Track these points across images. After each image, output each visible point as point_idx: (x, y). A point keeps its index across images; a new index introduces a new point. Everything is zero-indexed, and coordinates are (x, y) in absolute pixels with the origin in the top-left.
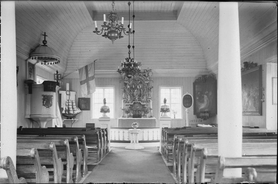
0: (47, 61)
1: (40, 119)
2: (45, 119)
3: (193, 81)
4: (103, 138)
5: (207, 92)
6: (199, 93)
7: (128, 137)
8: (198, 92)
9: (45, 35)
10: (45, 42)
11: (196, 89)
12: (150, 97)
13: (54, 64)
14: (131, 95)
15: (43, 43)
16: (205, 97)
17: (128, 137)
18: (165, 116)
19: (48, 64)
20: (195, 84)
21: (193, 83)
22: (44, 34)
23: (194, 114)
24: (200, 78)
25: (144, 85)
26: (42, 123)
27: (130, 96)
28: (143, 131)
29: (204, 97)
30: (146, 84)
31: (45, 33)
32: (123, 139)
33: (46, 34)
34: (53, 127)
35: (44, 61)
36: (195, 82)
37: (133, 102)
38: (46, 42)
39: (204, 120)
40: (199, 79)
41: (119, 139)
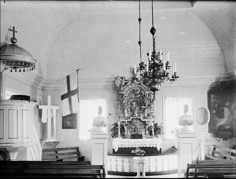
0: (17, 67)
1: (8, 149)
2: (15, 150)
3: (207, 89)
4: (233, 164)
5: (229, 104)
6: (216, 105)
7: (128, 168)
8: (215, 103)
9: (14, 31)
10: (13, 40)
11: (212, 100)
12: (152, 112)
13: (30, 70)
14: (128, 109)
15: (12, 42)
16: (225, 111)
17: (128, 168)
18: (100, 132)
19: (20, 71)
20: (210, 93)
21: (208, 92)
22: (12, 29)
23: (210, 131)
24: (218, 85)
25: (145, 96)
26: (11, 154)
27: (128, 110)
28: (162, 159)
29: (224, 110)
30: (147, 95)
31: (14, 27)
32: (122, 170)
33: (15, 30)
34: (28, 160)
35: (13, 67)
36: (210, 90)
37: (131, 118)
38: (16, 39)
39: (224, 140)
40: (217, 86)
41: (116, 170)
